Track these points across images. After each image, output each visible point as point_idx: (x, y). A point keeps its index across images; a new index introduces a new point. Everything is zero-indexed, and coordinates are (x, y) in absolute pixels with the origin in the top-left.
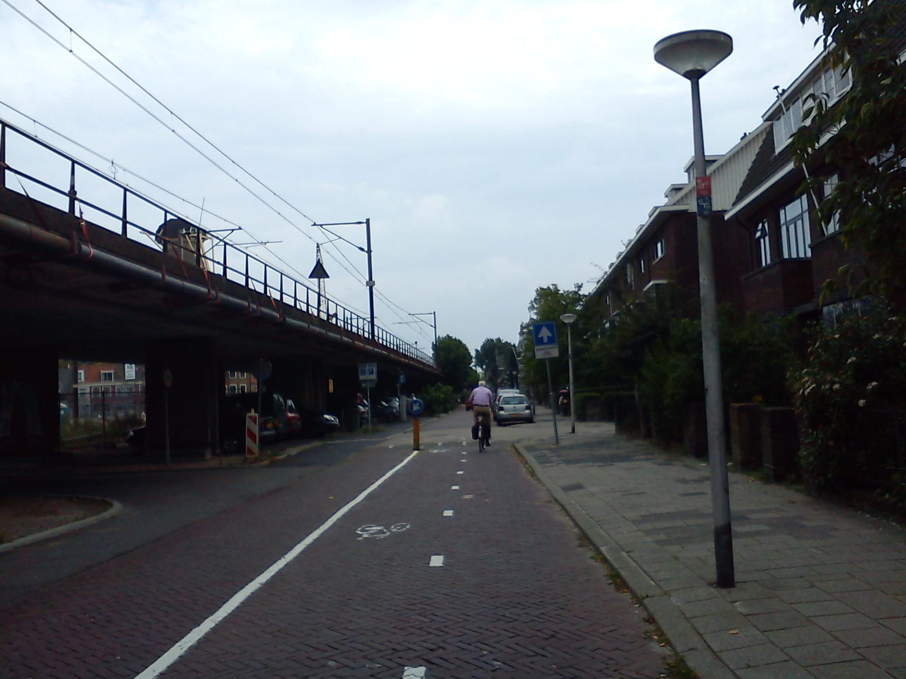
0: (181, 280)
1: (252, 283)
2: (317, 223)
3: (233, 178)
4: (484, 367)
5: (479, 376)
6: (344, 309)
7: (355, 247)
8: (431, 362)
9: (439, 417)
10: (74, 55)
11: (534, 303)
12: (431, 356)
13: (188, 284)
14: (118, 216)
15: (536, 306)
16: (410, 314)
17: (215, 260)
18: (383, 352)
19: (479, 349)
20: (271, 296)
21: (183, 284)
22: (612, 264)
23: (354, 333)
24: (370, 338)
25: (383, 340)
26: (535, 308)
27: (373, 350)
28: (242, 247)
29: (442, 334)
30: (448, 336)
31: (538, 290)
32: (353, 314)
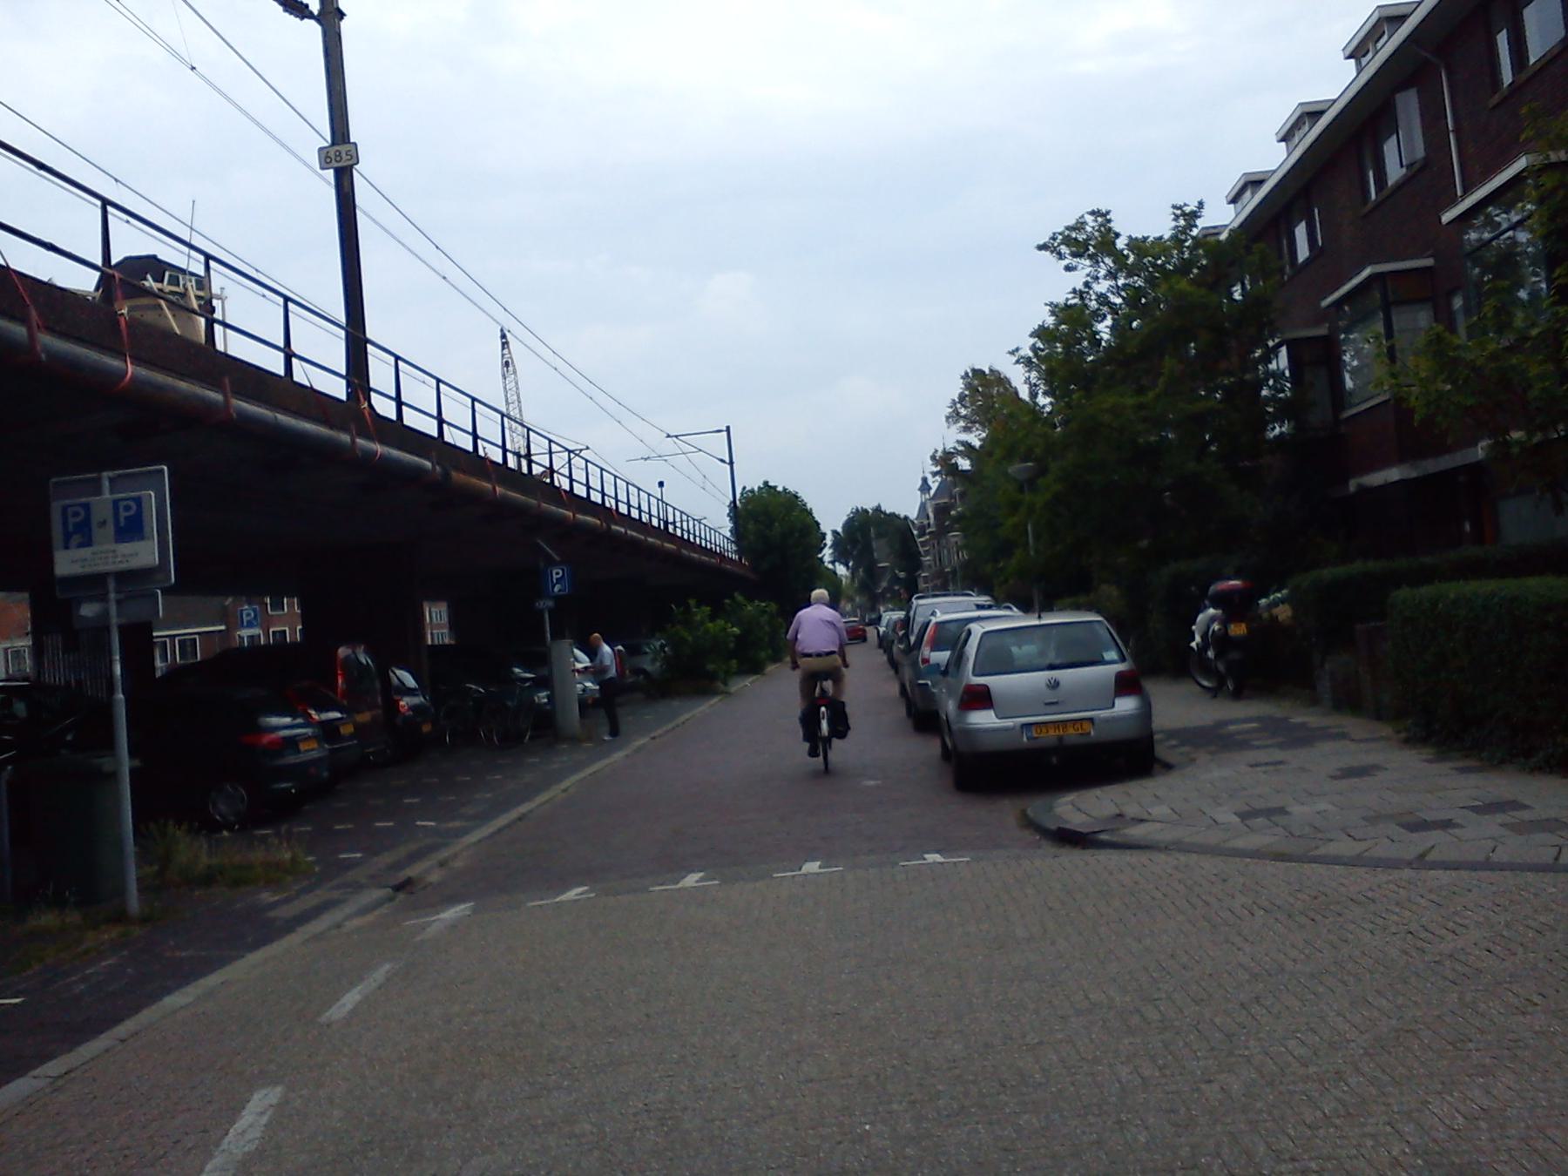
0: (271, 411)
1: (302, 366)
2: (671, 434)
3: (439, 274)
4: (851, 564)
5: (841, 581)
6: (602, 469)
7: (715, 460)
8: (730, 550)
9: (728, 694)
10: (448, 282)
11: (959, 406)
12: (728, 534)
13: (281, 417)
14: (388, 393)
15: (963, 412)
16: (669, 436)
17: (228, 321)
18: (703, 558)
19: (840, 530)
20: (561, 486)
21: (276, 417)
22: (1253, 183)
23: (634, 519)
24: (662, 527)
25: (701, 538)
26: (961, 417)
27: (700, 559)
28: (510, 428)
29: (750, 480)
30: (766, 483)
31: (967, 374)
32: (552, 444)
